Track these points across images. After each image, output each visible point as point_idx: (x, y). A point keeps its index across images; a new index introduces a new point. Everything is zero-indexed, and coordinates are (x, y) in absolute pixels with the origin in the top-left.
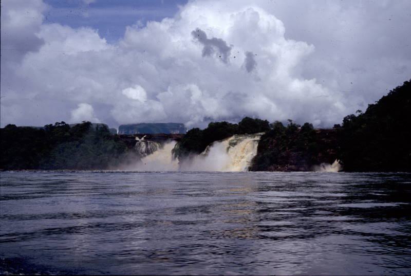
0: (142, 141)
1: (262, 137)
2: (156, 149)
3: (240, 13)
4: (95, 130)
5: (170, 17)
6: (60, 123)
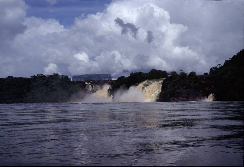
0: (90, 85)
1: (164, 81)
2: (98, 89)
3: (142, 8)
4: (61, 78)
5: (101, 12)
6: (39, 75)
